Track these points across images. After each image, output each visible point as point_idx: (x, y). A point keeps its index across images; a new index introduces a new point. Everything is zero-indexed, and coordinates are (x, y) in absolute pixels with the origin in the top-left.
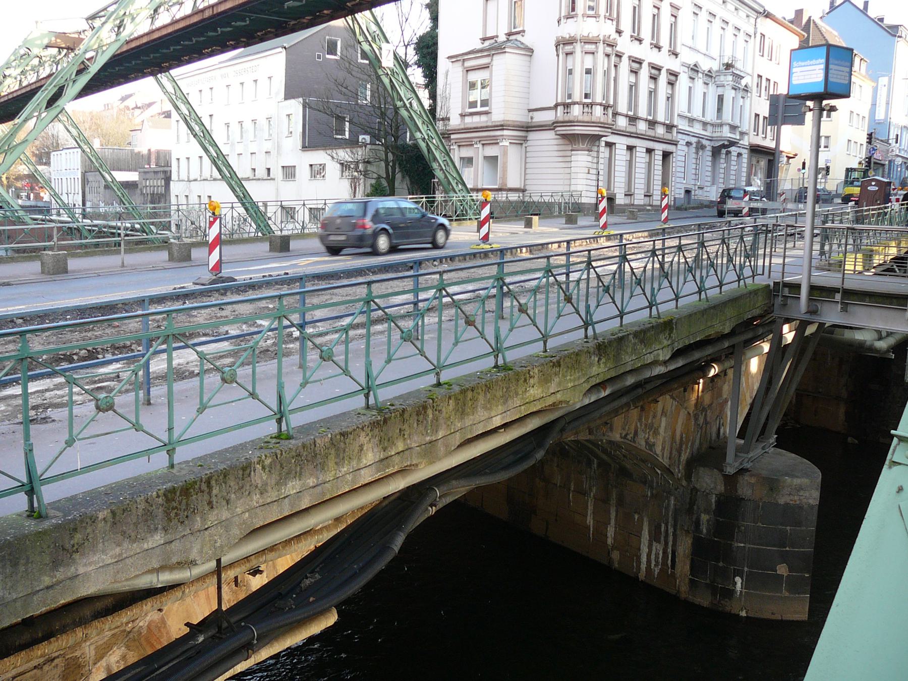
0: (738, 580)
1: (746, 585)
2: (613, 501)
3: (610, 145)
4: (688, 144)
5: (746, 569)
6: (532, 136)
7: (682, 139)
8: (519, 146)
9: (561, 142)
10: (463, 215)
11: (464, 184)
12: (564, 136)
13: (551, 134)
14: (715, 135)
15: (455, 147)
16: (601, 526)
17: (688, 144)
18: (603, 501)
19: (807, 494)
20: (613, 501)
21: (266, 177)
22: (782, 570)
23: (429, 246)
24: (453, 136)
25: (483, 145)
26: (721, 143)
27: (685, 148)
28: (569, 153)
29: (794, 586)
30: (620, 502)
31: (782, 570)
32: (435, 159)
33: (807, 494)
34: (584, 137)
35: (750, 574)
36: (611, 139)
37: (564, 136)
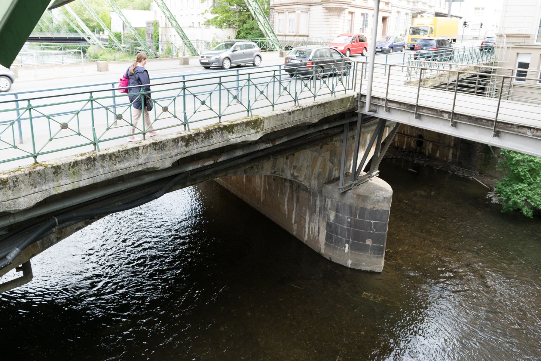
0: (347, 245)
1: (351, 248)
2: (295, 200)
3: (352, 13)
4: (407, 14)
5: (351, 240)
6: (312, 8)
7: (394, 10)
8: (306, 13)
9: (326, 11)
10: (265, 49)
11: (273, 33)
12: (327, 8)
13: (320, 8)
14: (414, 7)
15: (277, 13)
16: (290, 211)
17: (407, 14)
18: (291, 199)
19: (382, 205)
20: (295, 200)
21: (198, 26)
22: (369, 242)
23: (252, 65)
24: (275, 8)
25: (329, 9)
26: (417, 12)
27: (405, 16)
28: (329, 17)
29: (378, 251)
30: (298, 201)
31: (369, 242)
32: (259, 20)
33: (382, 205)
34: (336, 9)
35: (352, 243)
36: (352, 9)
37: (327, 8)
